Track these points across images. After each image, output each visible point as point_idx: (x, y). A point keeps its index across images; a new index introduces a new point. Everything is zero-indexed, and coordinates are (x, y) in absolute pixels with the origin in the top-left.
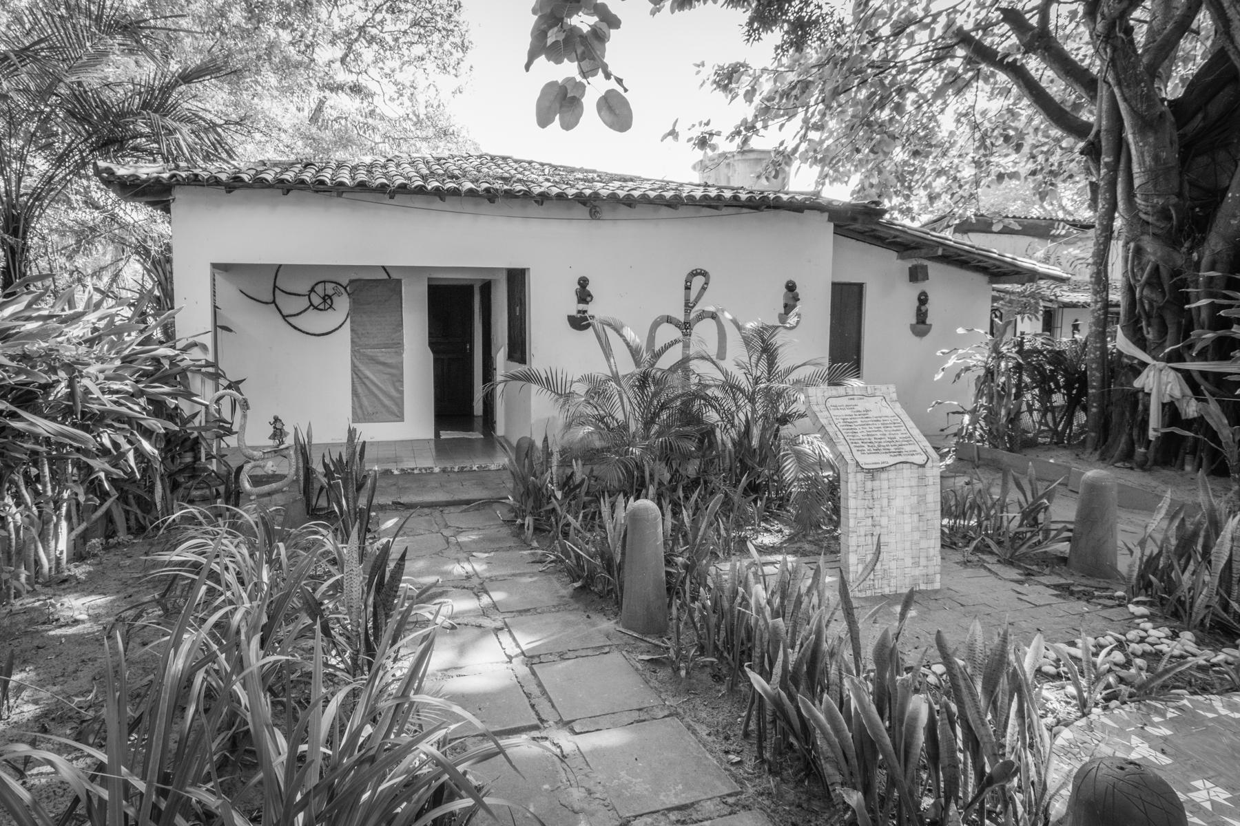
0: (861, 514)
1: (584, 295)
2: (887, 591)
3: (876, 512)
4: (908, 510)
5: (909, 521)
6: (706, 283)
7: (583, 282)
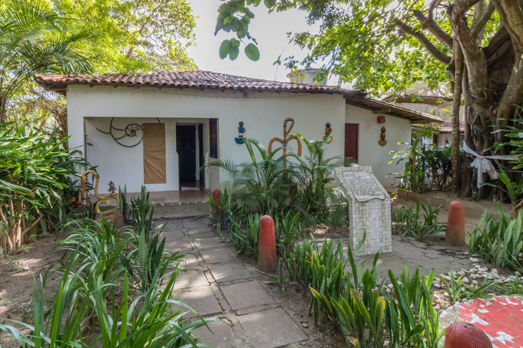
0: (358, 220)
1: (242, 130)
3: (364, 220)
4: (377, 219)
5: (378, 223)
6: (293, 124)
7: (241, 124)
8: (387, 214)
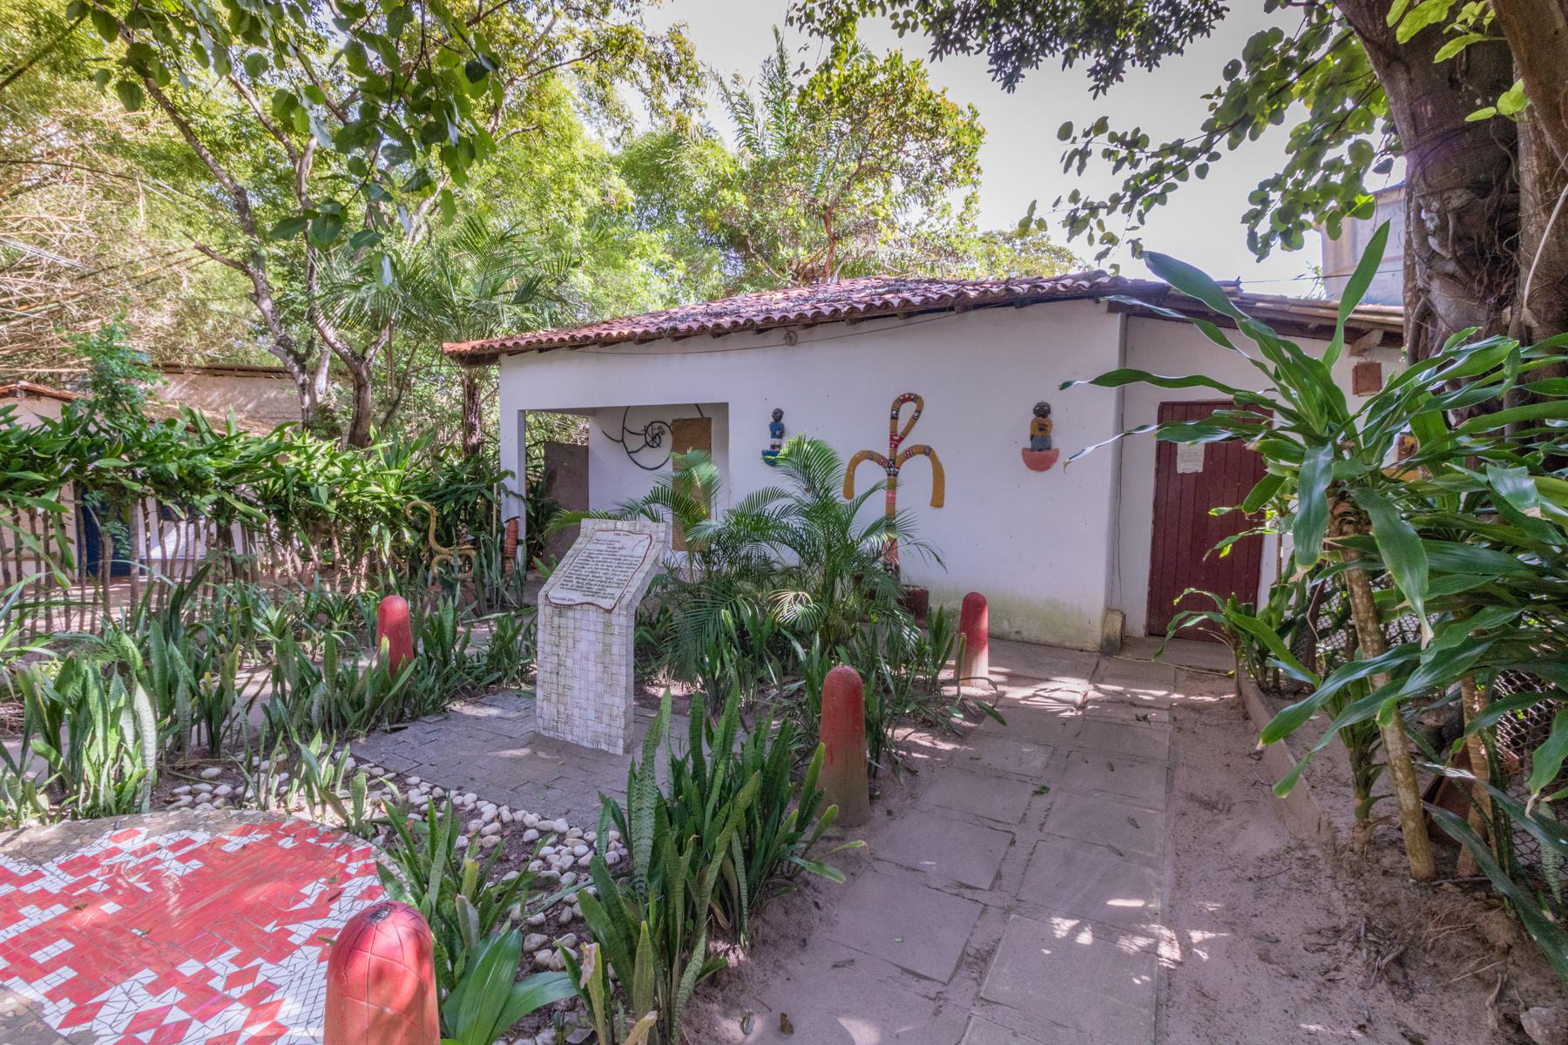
0: (548, 649)
1: (777, 429)
2: (569, 738)
3: (562, 652)
4: (592, 657)
5: (593, 671)
6: (919, 411)
7: (778, 415)
8: (615, 649)
